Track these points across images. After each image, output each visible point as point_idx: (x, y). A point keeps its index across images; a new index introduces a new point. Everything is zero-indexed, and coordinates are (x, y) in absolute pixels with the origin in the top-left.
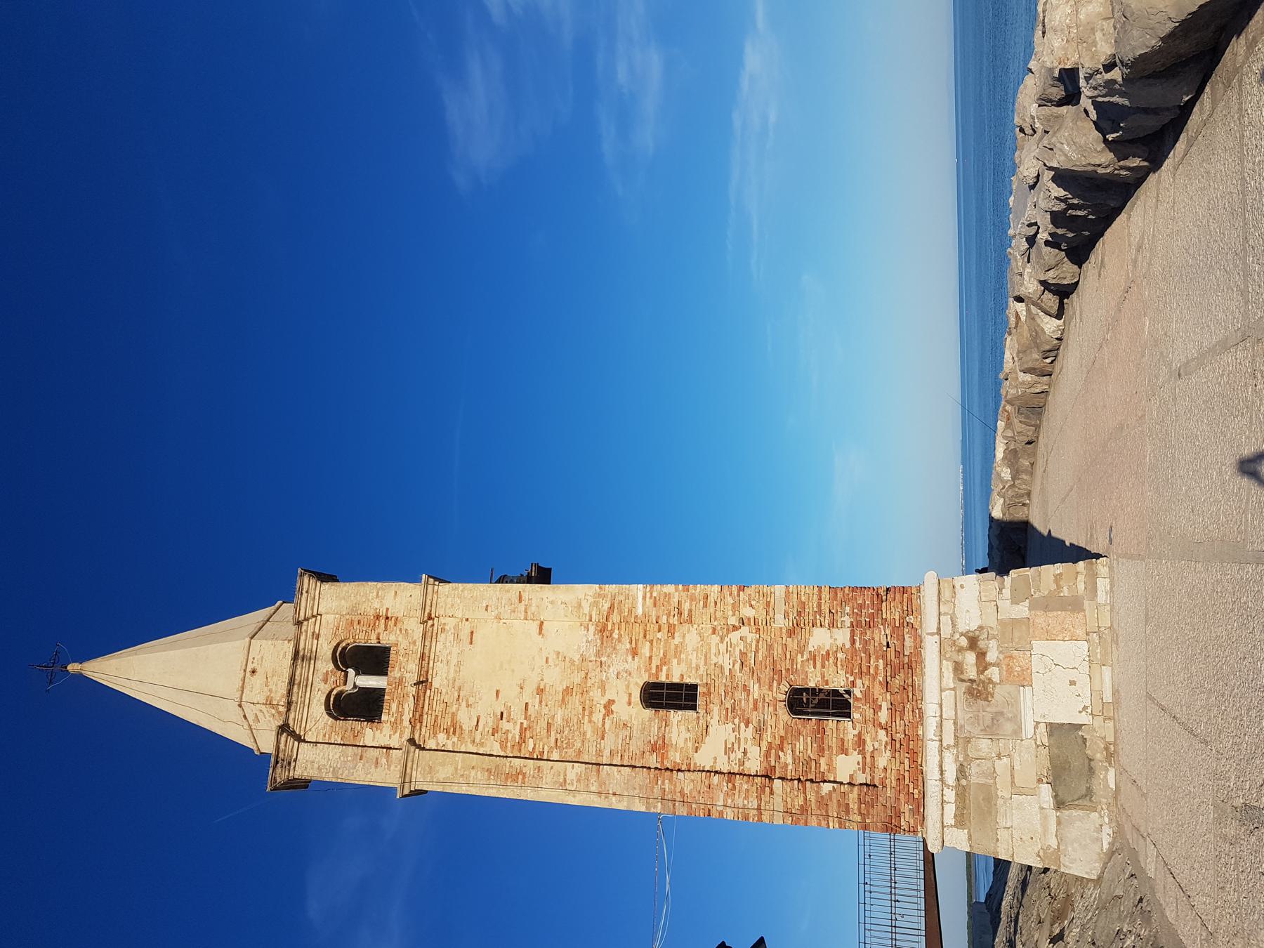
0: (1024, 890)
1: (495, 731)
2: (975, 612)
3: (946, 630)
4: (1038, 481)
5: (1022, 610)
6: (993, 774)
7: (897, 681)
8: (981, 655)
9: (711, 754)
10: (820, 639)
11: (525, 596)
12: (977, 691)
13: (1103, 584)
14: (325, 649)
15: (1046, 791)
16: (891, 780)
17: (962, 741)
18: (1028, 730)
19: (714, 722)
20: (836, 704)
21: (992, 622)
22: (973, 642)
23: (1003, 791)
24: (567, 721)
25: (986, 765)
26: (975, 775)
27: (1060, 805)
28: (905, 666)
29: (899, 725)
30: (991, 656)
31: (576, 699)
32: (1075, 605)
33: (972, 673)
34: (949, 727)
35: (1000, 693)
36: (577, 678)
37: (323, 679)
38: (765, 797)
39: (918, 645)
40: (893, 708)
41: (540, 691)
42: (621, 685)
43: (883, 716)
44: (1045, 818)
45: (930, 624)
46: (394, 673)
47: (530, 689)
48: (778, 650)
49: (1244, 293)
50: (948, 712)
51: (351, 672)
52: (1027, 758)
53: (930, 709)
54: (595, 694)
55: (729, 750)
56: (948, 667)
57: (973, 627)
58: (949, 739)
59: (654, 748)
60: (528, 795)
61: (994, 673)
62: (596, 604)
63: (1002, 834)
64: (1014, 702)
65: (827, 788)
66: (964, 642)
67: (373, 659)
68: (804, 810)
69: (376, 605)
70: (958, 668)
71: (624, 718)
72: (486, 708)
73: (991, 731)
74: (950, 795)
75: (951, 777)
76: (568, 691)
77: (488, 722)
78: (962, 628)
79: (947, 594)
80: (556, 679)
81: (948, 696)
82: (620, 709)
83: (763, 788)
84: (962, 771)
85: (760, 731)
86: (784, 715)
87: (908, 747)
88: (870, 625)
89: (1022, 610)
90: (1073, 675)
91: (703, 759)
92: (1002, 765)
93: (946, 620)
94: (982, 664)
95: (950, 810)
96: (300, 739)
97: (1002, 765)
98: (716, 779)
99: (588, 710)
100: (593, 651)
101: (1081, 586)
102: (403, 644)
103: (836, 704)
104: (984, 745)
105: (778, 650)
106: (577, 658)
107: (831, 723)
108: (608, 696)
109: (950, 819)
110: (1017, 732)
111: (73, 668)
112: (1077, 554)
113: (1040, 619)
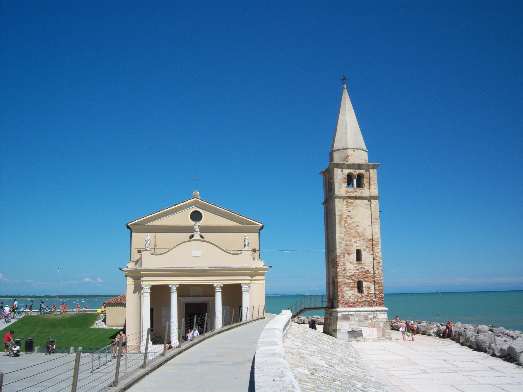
0: (511, 337)
1: (348, 216)
2: (381, 317)
8: (373, 318)
11: (377, 221)
12: (366, 318)
15: (351, 330)
19: (355, 265)
20: (360, 291)
23: (349, 322)
24: (352, 233)
26: (351, 317)
27: (348, 332)
29: (358, 303)
30: (373, 320)
32: (383, 336)
33: (370, 317)
36: (360, 234)
42: (360, 245)
43: (360, 300)
46: (358, 189)
49: (397, 377)
52: (355, 327)
54: (358, 239)
60: (337, 226)
63: (342, 322)
67: (360, 185)
72: (353, 213)
73: (360, 321)
76: (358, 232)
77: (350, 214)
85: (354, 275)
87: (354, 305)
89: (382, 326)
91: (348, 264)
94: (371, 319)
97: (353, 322)
103: (360, 291)
104: (357, 319)
108: (358, 242)
110: (359, 325)
111: (345, 86)
113: (381, 329)
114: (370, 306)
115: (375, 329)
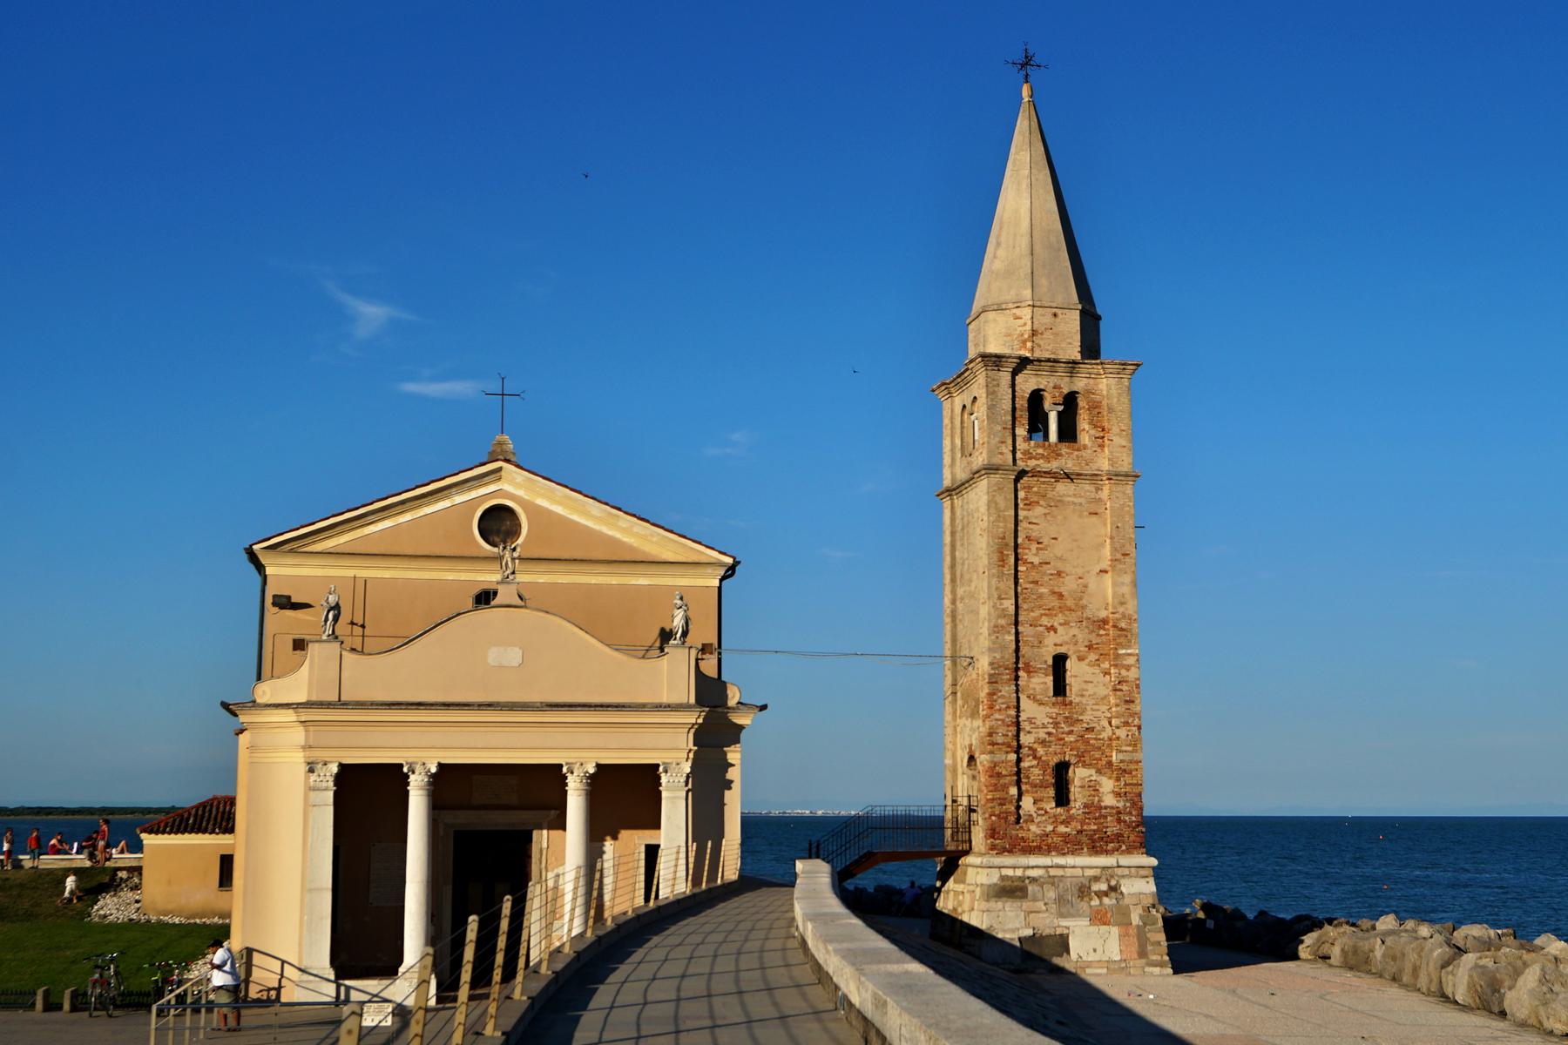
2: (1133, 890)
3: (1119, 871)
4: (985, 860)
5: (1135, 919)
6: (1035, 900)
7: (1084, 839)
8: (1106, 894)
9: (1029, 708)
10: (1107, 785)
11: (1127, 559)
12: (1083, 891)
13: (1157, 970)
14: (1080, 384)
15: (1029, 932)
16: (1021, 834)
17: (1053, 881)
18: (1064, 923)
19: (1048, 709)
20: (1062, 798)
21: (1127, 901)
22: (1113, 889)
23: (1026, 905)
24: (1040, 596)
25: (1040, 895)
28: (1097, 845)
30: (1106, 900)
31: (1055, 603)
32: (1142, 954)
33: (1096, 887)
34: (1060, 872)
35: (1084, 905)
36: (1070, 603)
37: (1052, 385)
38: (1004, 748)
39: (1107, 852)
40: (1067, 835)
41: (1059, 574)
42: (1066, 638)
43: (1062, 829)
44: (1013, 931)
45: (1126, 860)
46: (1064, 449)
47: (1060, 566)
48: (1097, 754)
50: (1069, 872)
51: (1061, 408)
53: (1070, 860)
55: (1030, 720)
56: (1097, 872)
57: (1123, 889)
58: (1053, 872)
59: (1027, 665)
61: (1095, 902)
62: (1124, 616)
64: (1077, 915)
65: (1014, 791)
66: (1113, 883)
68: (999, 775)
69: (1115, 430)
70: (1096, 879)
71: (1046, 642)
73: (1061, 900)
74: (1019, 873)
75: (1031, 873)
76: (1061, 596)
78: (1122, 882)
79: (1142, 872)
80: (1068, 585)
81: (1079, 872)
82: (1051, 639)
83: (1009, 746)
84: (1034, 880)
85: (1043, 742)
86: (1056, 759)
87: (1041, 847)
88: (1119, 821)
89: (1135, 919)
90: (1100, 950)
91: (1025, 703)
92: (1040, 905)
93: (1126, 872)
95: (1010, 872)
96: (1015, 373)
97: (1040, 905)
98: (1013, 712)
99: (1050, 612)
100: (1088, 613)
101: (1154, 958)
102: (1086, 454)
103: (1062, 798)
104: (1051, 894)
105: (1097, 754)
106: (1084, 602)
107: (1052, 792)
108: (1060, 629)
109: (1005, 872)
110: (1061, 915)
112: (307, 606)
114: (1095, 850)
115: (1115, 930)
